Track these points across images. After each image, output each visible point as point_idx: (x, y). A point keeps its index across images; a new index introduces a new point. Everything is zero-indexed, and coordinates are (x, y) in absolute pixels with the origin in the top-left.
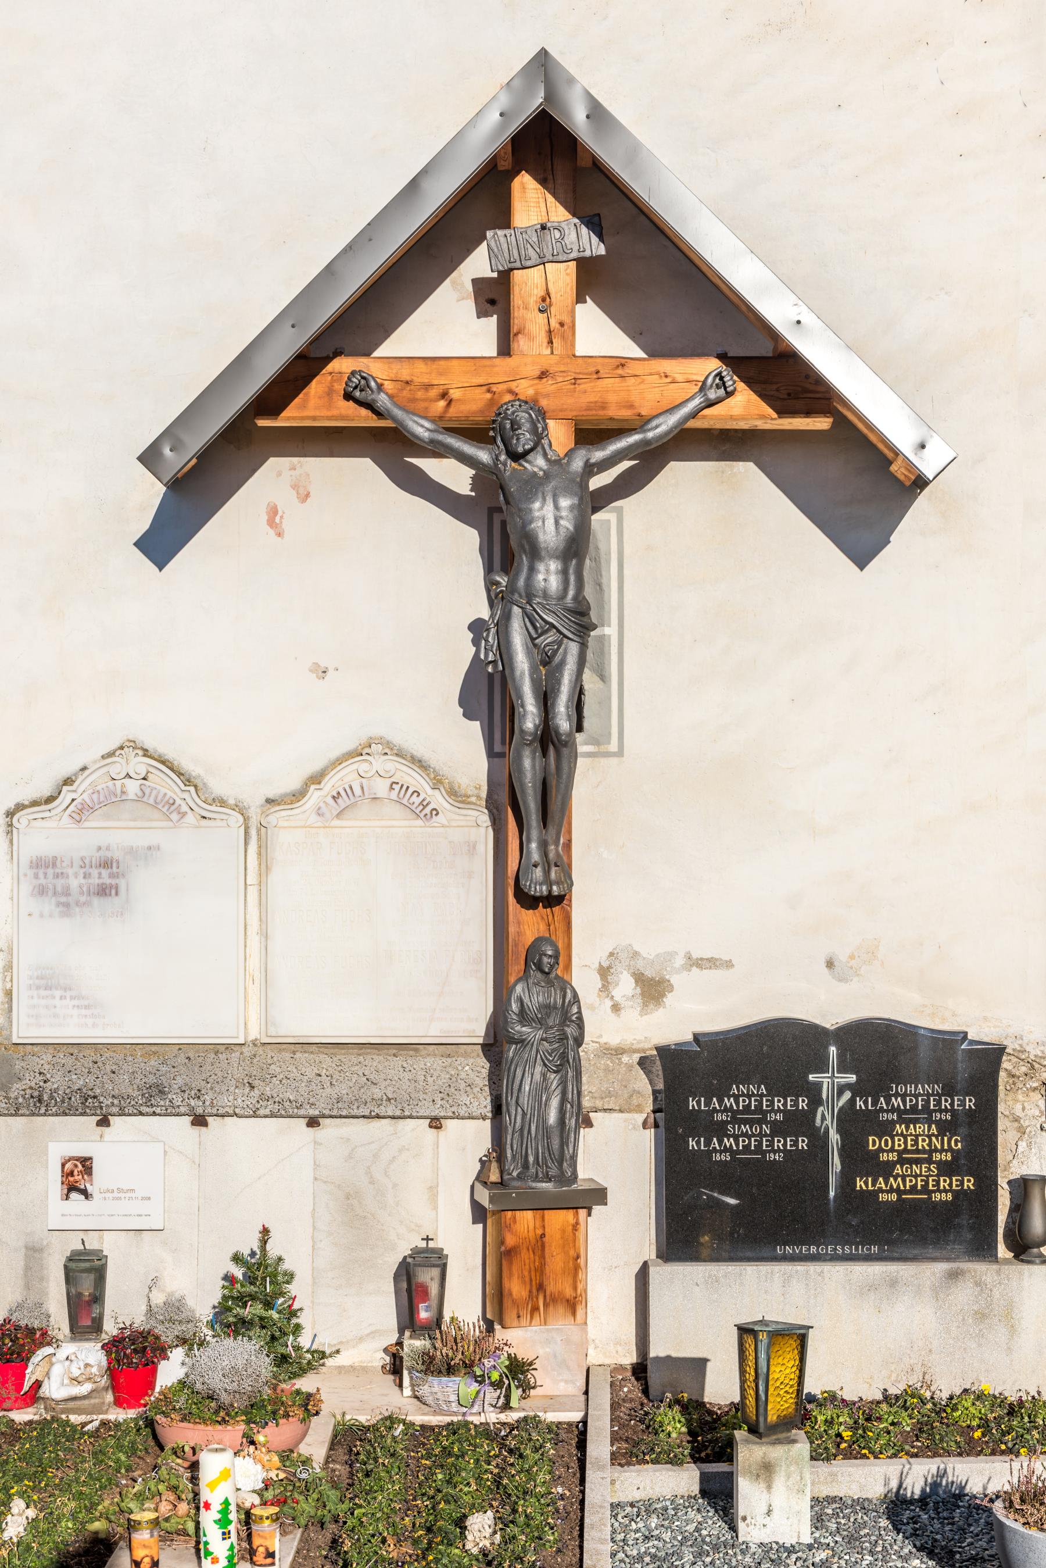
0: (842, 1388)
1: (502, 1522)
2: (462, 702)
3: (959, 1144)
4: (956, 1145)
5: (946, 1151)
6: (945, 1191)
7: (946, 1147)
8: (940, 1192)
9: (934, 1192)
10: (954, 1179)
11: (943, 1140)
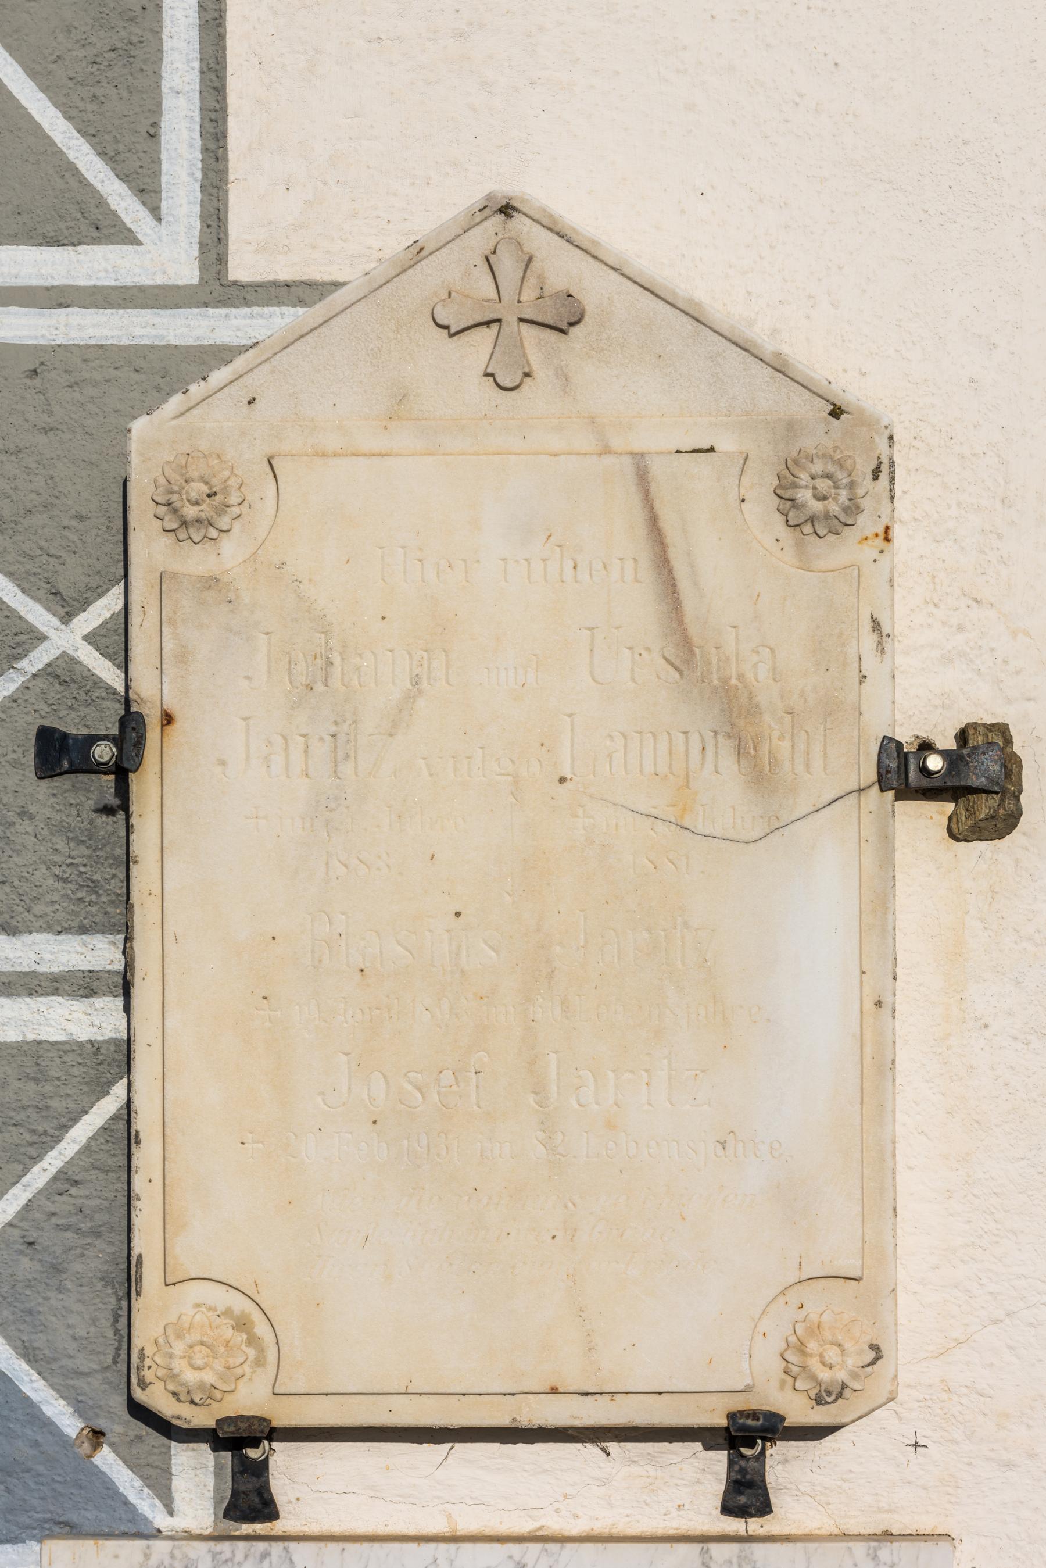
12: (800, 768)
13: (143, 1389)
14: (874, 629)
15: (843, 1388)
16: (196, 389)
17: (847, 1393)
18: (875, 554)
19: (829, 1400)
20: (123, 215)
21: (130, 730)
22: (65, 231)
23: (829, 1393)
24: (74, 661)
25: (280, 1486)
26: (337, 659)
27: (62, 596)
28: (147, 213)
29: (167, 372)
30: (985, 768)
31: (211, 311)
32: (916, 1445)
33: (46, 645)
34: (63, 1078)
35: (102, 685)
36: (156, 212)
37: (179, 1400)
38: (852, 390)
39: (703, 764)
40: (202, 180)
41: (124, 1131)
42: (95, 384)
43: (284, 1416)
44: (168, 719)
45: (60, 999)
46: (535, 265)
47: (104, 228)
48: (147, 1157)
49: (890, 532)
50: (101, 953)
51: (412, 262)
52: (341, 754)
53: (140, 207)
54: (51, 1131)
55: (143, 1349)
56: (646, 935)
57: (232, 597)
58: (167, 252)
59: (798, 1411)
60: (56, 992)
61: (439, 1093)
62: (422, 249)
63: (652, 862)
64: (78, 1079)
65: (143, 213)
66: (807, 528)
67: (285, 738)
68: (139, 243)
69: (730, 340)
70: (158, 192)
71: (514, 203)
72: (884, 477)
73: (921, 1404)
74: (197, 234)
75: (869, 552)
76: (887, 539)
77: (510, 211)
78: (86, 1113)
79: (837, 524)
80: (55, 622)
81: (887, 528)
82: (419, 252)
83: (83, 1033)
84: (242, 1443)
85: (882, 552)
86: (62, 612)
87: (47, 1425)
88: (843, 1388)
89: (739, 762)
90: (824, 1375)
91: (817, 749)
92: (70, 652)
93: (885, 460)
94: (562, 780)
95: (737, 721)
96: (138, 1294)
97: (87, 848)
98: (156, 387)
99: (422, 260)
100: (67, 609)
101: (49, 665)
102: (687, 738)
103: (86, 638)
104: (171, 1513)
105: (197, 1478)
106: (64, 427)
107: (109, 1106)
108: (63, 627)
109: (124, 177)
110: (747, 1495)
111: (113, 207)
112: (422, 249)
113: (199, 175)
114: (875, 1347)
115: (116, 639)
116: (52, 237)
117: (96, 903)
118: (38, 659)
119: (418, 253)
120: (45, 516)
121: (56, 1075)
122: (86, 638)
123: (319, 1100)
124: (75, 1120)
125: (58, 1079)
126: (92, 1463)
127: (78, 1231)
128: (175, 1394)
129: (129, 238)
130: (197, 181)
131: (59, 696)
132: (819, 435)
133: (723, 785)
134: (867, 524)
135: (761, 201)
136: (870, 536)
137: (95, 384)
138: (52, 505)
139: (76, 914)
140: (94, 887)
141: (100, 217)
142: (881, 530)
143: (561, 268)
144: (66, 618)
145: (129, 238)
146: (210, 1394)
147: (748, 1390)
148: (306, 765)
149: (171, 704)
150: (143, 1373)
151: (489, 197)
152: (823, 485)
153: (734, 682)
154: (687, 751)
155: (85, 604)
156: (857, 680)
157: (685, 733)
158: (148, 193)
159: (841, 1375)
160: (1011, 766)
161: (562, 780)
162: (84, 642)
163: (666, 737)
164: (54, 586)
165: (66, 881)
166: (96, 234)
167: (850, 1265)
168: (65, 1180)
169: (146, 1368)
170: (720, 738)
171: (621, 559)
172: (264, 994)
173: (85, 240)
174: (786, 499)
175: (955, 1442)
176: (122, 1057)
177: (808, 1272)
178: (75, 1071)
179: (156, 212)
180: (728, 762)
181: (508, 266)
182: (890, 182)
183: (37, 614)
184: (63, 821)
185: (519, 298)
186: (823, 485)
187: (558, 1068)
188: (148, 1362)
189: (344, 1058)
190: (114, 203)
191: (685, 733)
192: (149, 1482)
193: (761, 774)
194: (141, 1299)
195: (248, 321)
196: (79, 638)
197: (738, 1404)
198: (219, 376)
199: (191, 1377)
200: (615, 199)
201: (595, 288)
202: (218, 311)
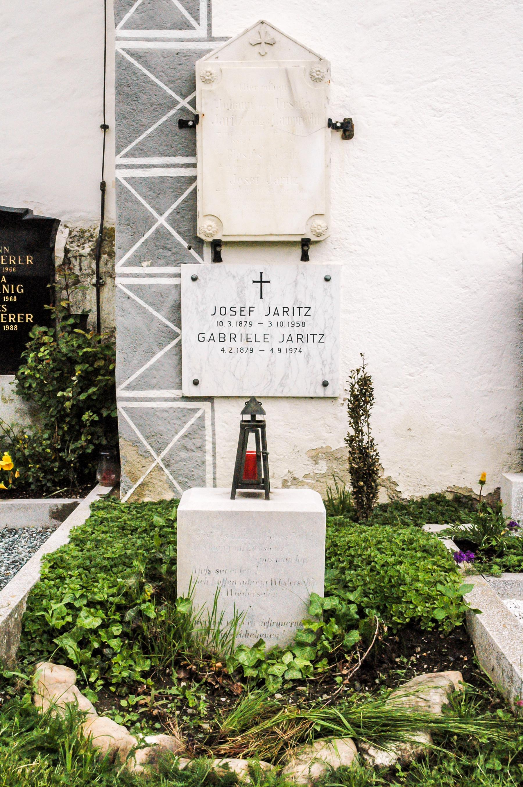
0: (325, 384)
1: (108, 367)
2: (351, 138)
3: (22, 291)
4: (20, 291)
5: (13, 295)
6: (13, 324)
7: (13, 292)
8: (10, 324)
9: (5, 324)
10: (19, 315)
11: (10, 287)
21: (197, 118)
25: (223, 256)
29: (200, 54)
30: (314, 453)
36: (199, 24)
38: (322, 54)
41: (196, 188)
43: (224, 239)
48: (199, 194)
50: (189, 160)
58: (201, 31)
59: (313, 238)
79: (321, 80)
82: (247, 31)
84: (216, 245)
87: (181, 245)
90: (318, 231)
95: (303, 116)
100: (184, 97)
105: (208, 252)
107: (191, 188)
109: (193, 17)
110: (305, 257)
115: (193, 103)
118: (179, 107)
129: (193, 28)
132: (318, 67)
134: (326, 80)
140: (189, 148)
144: (184, 99)
146: (212, 235)
149: (203, 112)
158: (197, 19)
159: (320, 231)
160: (352, 126)
168: (184, 201)
174: (312, 76)
176: (194, 179)
179: (199, 24)
181: (263, 35)
183: (178, 98)
185: (265, 40)
186: (318, 73)
190: (191, 22)
199: (208, 232)
200: (283, 22)
201: (278, 37)
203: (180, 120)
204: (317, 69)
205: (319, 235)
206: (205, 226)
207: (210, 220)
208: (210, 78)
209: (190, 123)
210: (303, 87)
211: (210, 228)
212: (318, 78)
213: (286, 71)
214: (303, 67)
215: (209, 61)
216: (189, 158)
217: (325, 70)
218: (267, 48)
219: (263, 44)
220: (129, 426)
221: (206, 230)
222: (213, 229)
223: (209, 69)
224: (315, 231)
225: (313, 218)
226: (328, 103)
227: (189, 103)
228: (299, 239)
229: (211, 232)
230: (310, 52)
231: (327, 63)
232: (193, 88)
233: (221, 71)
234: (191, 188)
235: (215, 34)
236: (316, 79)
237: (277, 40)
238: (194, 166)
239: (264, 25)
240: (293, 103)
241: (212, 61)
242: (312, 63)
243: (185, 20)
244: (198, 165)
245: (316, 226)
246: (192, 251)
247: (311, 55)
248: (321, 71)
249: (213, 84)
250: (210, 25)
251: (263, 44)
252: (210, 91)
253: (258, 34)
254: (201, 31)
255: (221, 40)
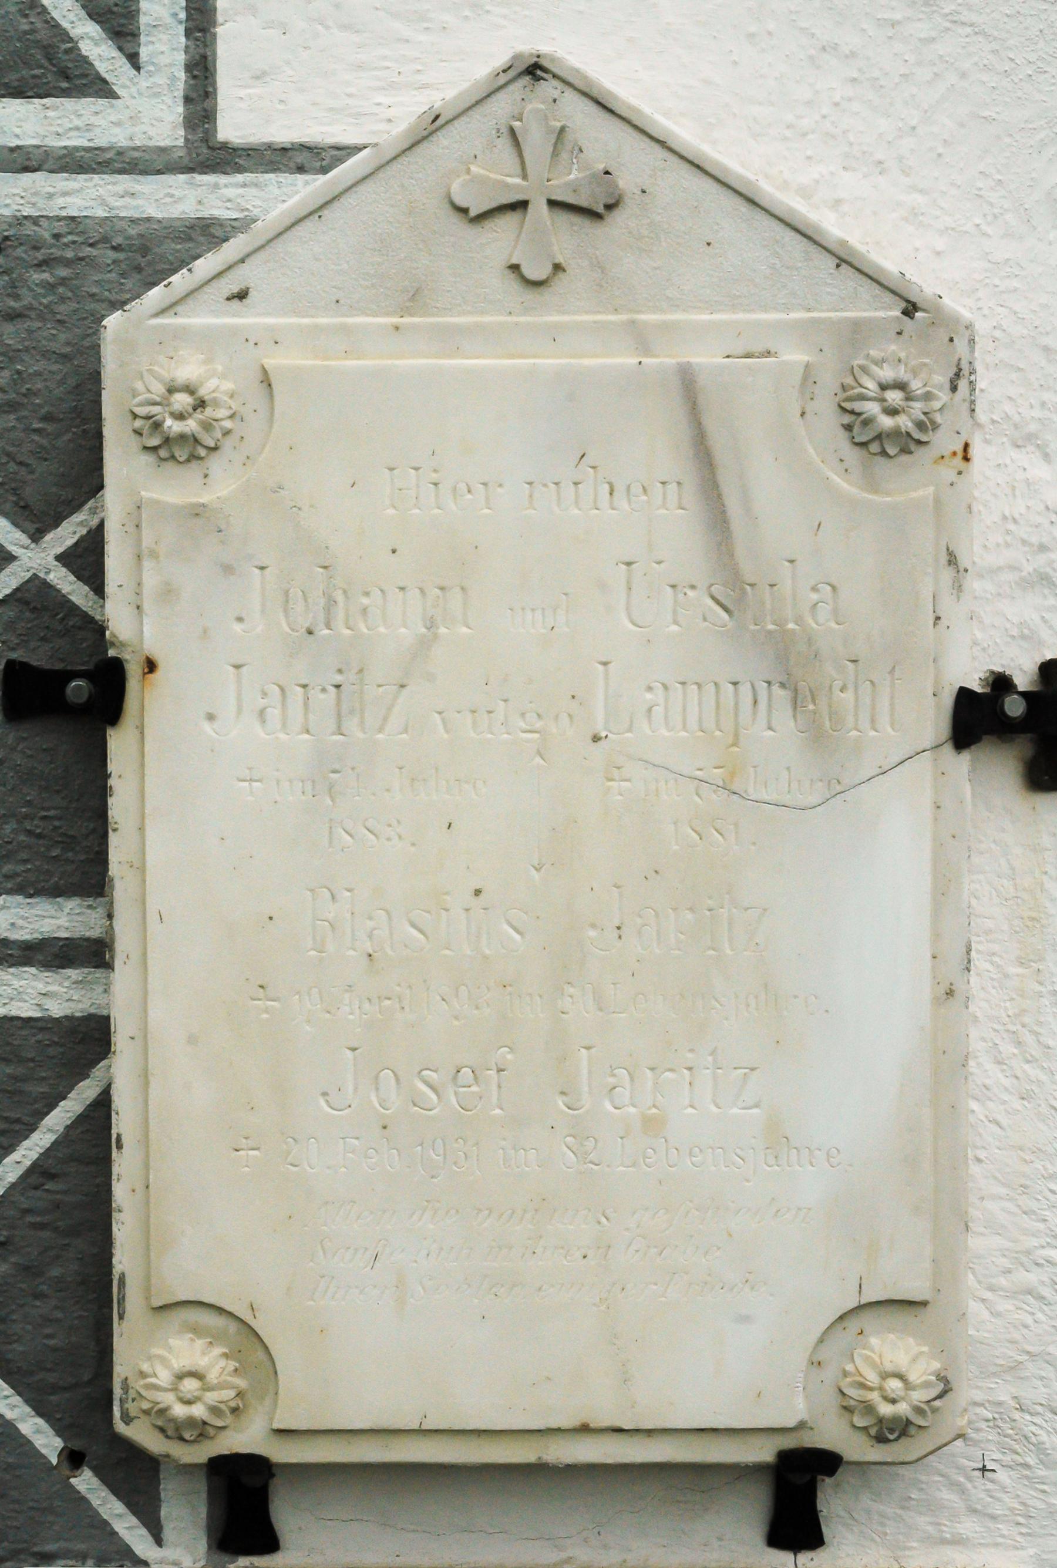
12: (865, 723)
13: (127, 1424)
14: (950, 563)
15: (907, 1425)
16: (179, 280)
17: (912, 1430)
18: (952, 475)
19: (891, 1437)
20: (97, 64)
22: (31, 81)
23: (892, 1431)
24: (46, 585)
26: (340, 597)
27: (32, 511)
28: (124, 60)
29: (149, 256)
31: (199, 178)
32: (984, 1469)
33: (13, 567)
34: (37, 1059)
35: (77, 612)
36: (134, 59)
37: (167, 1437)
38: (925, 282)
39: (754, 719)
40: (187, 20)
41: (103, 1104)
42: (68, 263)
43: (281, 1453)
44: (151, 666)
45: (33, 970)
46: (569, 136)
47: (78, 80)
49: (970, 450)
51: (425, 133)
52: (345, 707)
53: (116, 53)
54: (26, 1119)
55: (126, 1379)
56: (689, 916)
57: (223, 527)
58: (147, 109)
60: (27, 962)
61: (456, 1093)
62: (437, 117)
63: (695, 831)
64: (55, 1061)
65: (122, 62)
66: (875, 447)
67: (282, 690)
68: (116, 96)
69: (788, 224)
70: (135, 35)
71: (544, 63)
72: (963, 384)
73: (991, 1424)
74: (181, 85)
75: (947, 473)
76: (966, 459)
77: (539, 72)
78: (64, 1098)
79: (907, 443)
80: (24, 539)
81: (966, 446)
82: (435, 123)
83: (57, 1009)
85: (960, 473)
86: (32, 528)
88: (907, 1425)
89: (794, 716)
90: (886, 1410)
91: (884, 703)
92: (42, 575)
93: (964, 365)
94: (596, 739)
95: (794, 674)
96: (121, 1317)
97: (63, 798)
98: (136, 268)
99: (437, 130)
100: (38, 522)
101: (17, 590)
102: (736, 691)
103: (59, 558)
104: (159, 1542)
106: (33, 314)
107: (84, 1093)
108: (33, 546)
111: (84, 53)
112: (437, 117)
113: (183, 15)
114: (945, 1380)
115: (88, 559)
116: (15, 88)
117: (73, 862)
119: (434, 121)
120: (12, 417)
121: (30, 1056)
122: (59, 558)
123: (322, 1102)
124: (52, 1106)
125: (32, 1060)
126: (65, 1441)
127: (56, 1229)
128: (162, 1430)
129: (102, 89)
130: (181, 22)
131: (29, 625)
132: (890, 359)
133: (774, 737)
134: (945, 441)
135: (824, 49)
136: (946, 454)
137: (68, 263)
138: (19, 404)
139: (49, 873)
141: (70, 65)
142: (959, 448)
143: (600, 141)
144: (36, 536)
145: (102, 89)
146: (202, 1430)
147: (802, 1426)
148: (306, 719)
149: (152, 642)
150: (126, 1406)
151: (517, 57)
152: (894, 397)
153: (791, 626)
154: (737, 704)
155: (56, 522)
156: (931, 622)
157: (735, 684)
158: (123, 30)
159: (903, 1409)
161: (596, 739)
162: (56, 563)
163: (712, 688)
164: (23, 499)
165: (39, 836)
166: (65, 85)
167: (913, 1288)
169: (130, 1400)
170: (775, 688)
171: (663, 483)
172: (260, 983)
173: (53, 92)
175: (1026, 1466)
177: (869, 1296)
178: (51, 1051)
179: (134, 59)
180: (783, 715)
181: (536, 143)
182: (971, 25)
184: (35, 768)
185: (550, 181)
186: (894, 397)
187: (590, 1072)
188: (132, 1394)
189: (349, 1054)
190: (86, 48)
191: (735, 684)
192: (134, 1508)
193: (820, 734)
194: (125, 1323)
195: (241, 191)
196: (51, 559)
197: (789, 1443)
198: (205, 265)
199: (179, 1411)
201: (634, 165)
202: (205, 178)
203: (10, 664)
204: (887, 374)
205: (891, 1431)
206: (164, 1377)
207: (196, 1330)
208: (191, 425)
209: (78, 689)
210: (795, 491)
211: (190, 1385)
212: (896, 434)
213: (688, 383)
214: (795, 356)
215: (196, 319)
216: (72, 904)
217: (941, 379)
218: (566, 238)
219: (539, 209)
220: (270, 314)
221: (167, 1399)
222: (212, 1397)
223: (187, 371)
224: (869, 1409)
225: (853, 1325)
226: (958, 588)
227: (65, 559)
228: (764, 1453)
229: (198, 1411)
230: (844, 260)
231: (949, 330)
232: (86, 479)
233: (266, 381)
234: (84, 1093)
235: (232, 127)
236: (885, 434)
237: (626, 182)
238: (94, 954)
239: (548, 88)
240: (734, 590)
241: (206, 317)
242: (857, 333)
243: (43, 34)
244: (124, 944)
245: (872, 1377)
246: (85, 1482)
247: (848, 278)
248: (916, 386)
249: (216, 464)
250: (201, 71)
251: (539, 209)
252: (197, 512)
253: (504, 144)
254: (147, 109)
255: (273, 167)
